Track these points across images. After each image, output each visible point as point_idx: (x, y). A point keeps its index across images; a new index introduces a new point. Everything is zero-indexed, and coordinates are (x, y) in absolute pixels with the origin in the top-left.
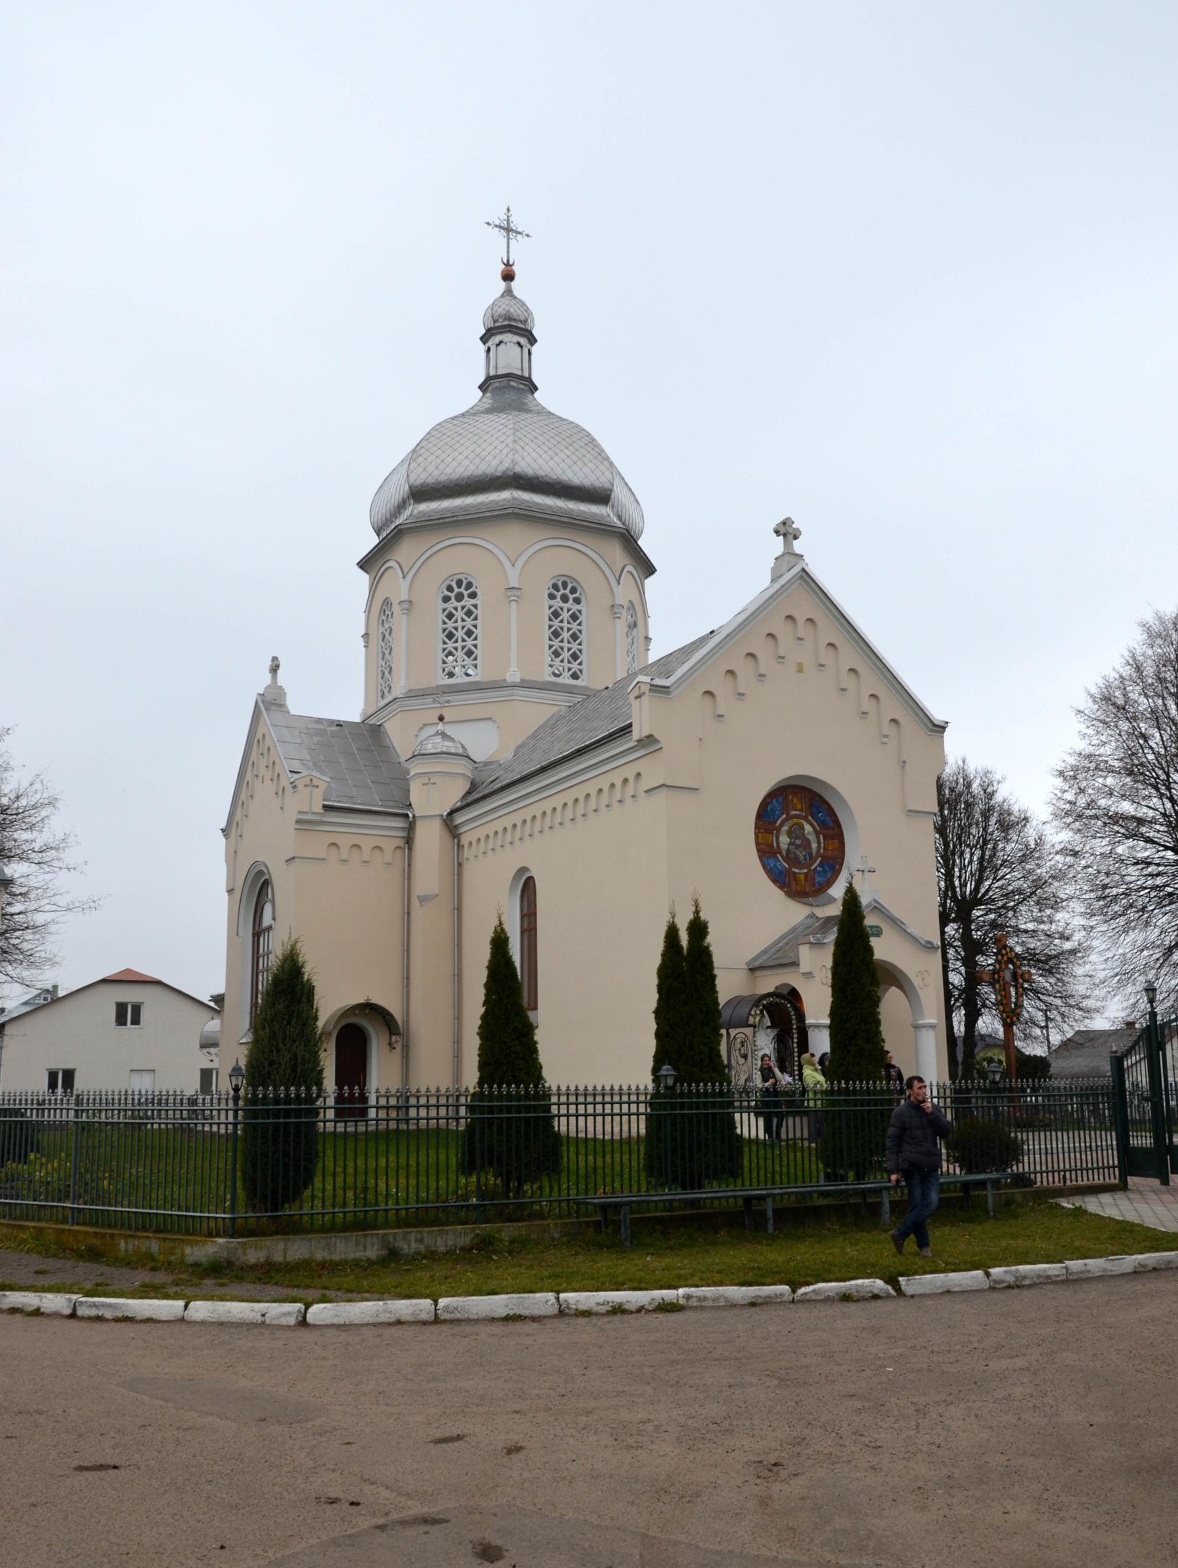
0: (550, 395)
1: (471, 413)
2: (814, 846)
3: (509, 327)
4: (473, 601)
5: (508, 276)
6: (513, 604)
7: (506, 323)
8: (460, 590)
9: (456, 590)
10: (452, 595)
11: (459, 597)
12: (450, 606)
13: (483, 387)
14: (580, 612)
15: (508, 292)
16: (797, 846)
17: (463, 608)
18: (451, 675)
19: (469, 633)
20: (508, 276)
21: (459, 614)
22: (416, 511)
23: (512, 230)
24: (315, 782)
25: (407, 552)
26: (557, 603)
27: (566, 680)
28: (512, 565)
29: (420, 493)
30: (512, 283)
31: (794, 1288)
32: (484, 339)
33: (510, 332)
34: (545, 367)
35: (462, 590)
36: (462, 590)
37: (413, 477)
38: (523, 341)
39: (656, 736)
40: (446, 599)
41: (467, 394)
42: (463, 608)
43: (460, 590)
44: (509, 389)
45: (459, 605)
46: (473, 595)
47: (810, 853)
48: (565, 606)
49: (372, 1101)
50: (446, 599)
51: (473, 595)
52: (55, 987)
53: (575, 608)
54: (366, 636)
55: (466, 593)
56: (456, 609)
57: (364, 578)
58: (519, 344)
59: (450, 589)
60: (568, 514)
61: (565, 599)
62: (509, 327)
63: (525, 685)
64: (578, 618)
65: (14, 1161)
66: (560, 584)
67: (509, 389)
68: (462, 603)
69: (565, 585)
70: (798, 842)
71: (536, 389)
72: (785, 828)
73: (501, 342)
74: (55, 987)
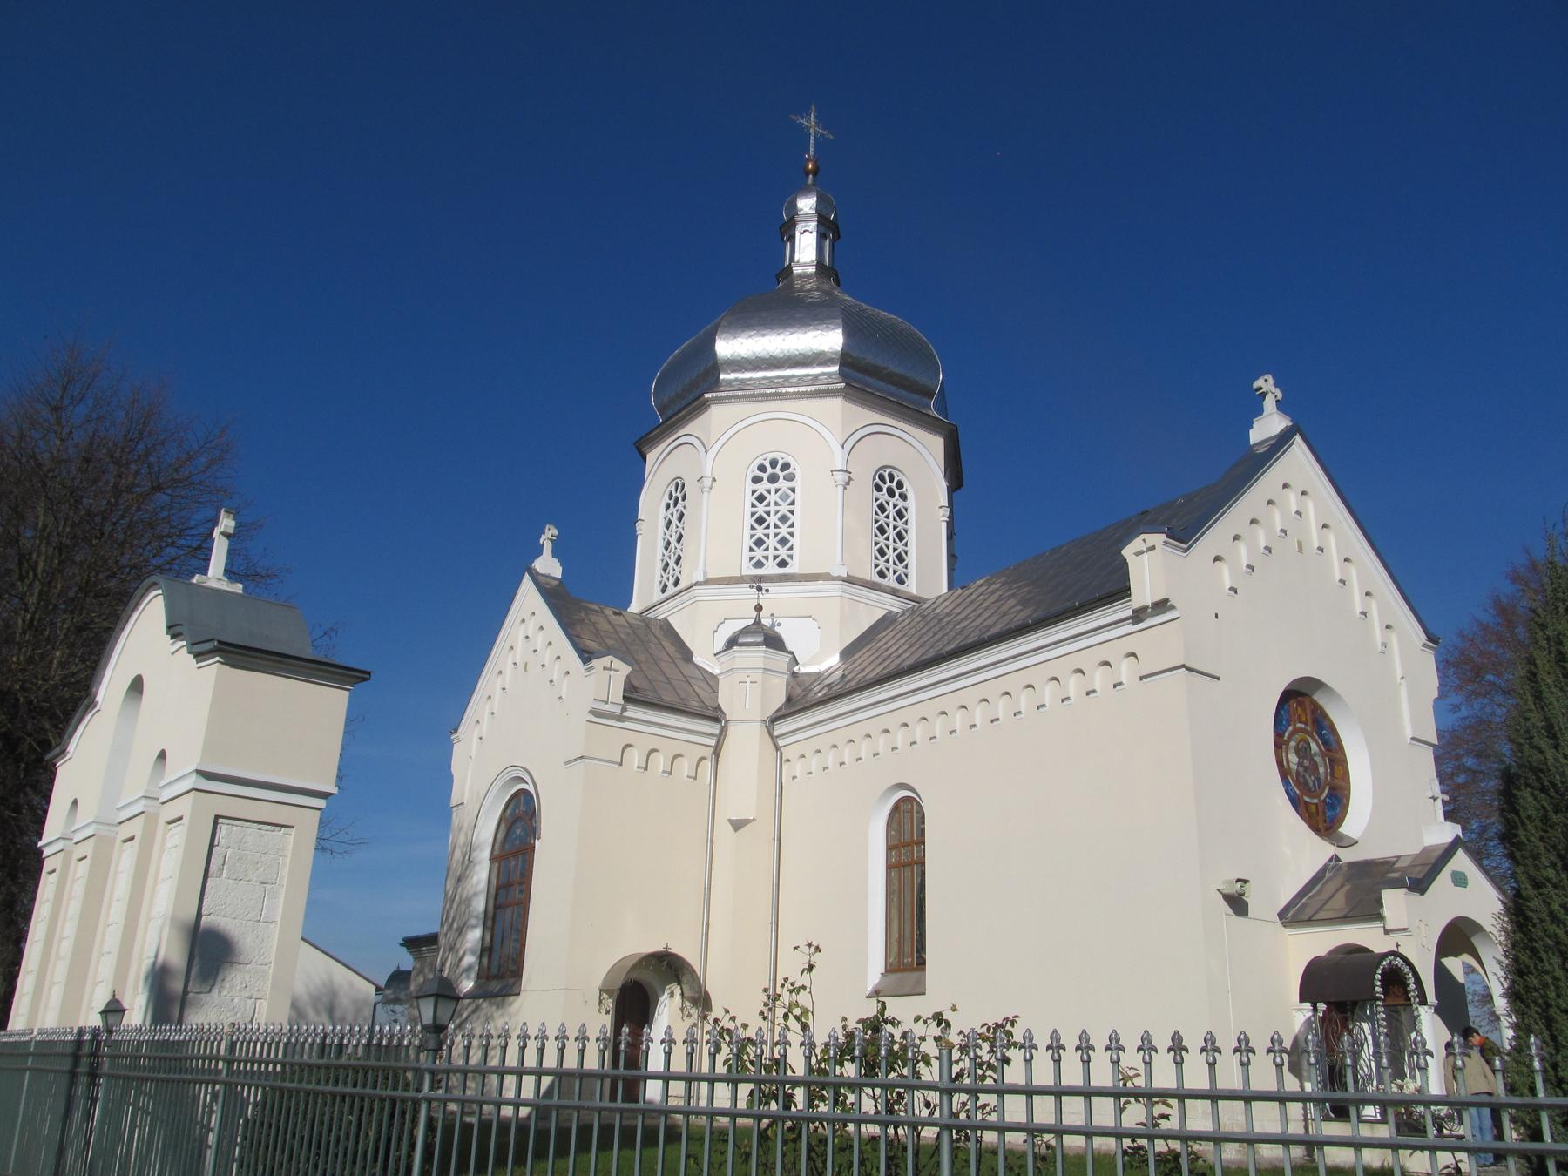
2: (1322, 770)
4: (790, 484)
10: (765, 476)
12: (761, 488)
16: (1306, 769)
18: (759, 564)
19: (784, 519)
26: (884, 496)
27: (890, 581)
31: (234, 1160)
35: (777, 470)
39: (1172, 602)
40: (756, 480)
45: (772, 487)
46: (790, 478)
47: (1319, 779)
48: (892, 501)
49: (656, 1062)
51: (790, 478)
53: (901, 504)
61: (891, 493)
65: (504, 1126)
68: (777, 485)
69: (882, 478)
70: (1306, 763)
72: (1293, 744)
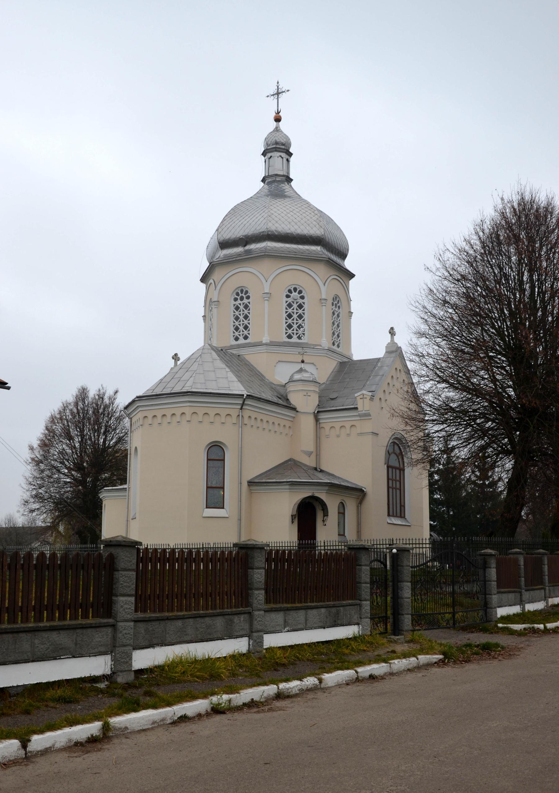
0: (299, 184)
1: (257, 196)
3: (278, 148)
5: (278, 119)
6: (266, 302)
7: (274, 146)
8: (242, 294)
9: (241, 295)
10: (239, 297)
11: (242, 299)
13: (263, 180)
14: (304, 303)
15: (277, 129)
17: (243, 304)
20: (278, 119)
21: (242, 307)
22: (222, 255)
23: (278, 96)
24: (365, 396)
25: (217, 275)
28: (267, 281)
29: (224, 245)
30: (280, 123)
32: (264, 154)
33: (276, 151)
34: (296, 170)
36: (243, 295)
37: (220, 236)
38: (283, 155)
40: (236, 300)
41: (256, 186)
42: (243, 304)
43: (242, 294)
44: (277, 183)
46: (248, 298)
50: (236, 300)
52: (207, 710)
54: (204, 316)
55: (245, 296)
56: (240, 304)
57: (203, 286)
58: (281, 156)
59: (237, 294)
60: (295, 252)
62: (278, 148)
63: (272, 344)
64: (303, 307)
66: (292, 289)
67: (277, 183)
68: (243, 302)
71: (292, 180)
73: (271, 157)
74: (207, 710)
